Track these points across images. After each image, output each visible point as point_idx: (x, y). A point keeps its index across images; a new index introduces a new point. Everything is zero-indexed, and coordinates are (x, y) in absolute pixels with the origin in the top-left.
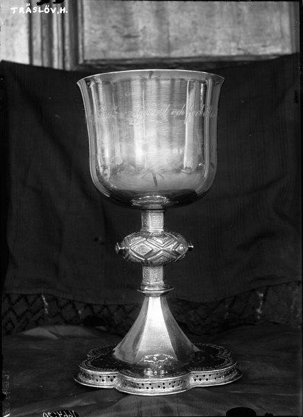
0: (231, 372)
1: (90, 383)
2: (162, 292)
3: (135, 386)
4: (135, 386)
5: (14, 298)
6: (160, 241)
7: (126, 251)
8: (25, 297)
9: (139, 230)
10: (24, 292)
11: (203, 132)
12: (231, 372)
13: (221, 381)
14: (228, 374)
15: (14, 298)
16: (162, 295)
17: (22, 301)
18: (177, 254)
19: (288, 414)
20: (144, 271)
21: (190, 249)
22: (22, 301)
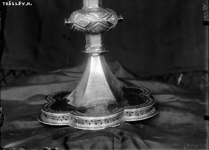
0: (151, 109)
1: (50, 122)
2: (101, 52)
3: (82, 122)
4: (82, 122)
5: (6, 72)
6: (96, 15)
7: (72, 24)
8: (13, 72)
9: (81, 8)
10: (13, 69)
11: (168, 100)
12: (151, 109)
13: (144, 117)
14: (149, 111)
15: (6, 72)
16: (101, 54)
17: (11, 74)
18: (110, 24)
19: (207, 62)
20: (86, 38)
21: (120, 21)
22: (11, 74)
